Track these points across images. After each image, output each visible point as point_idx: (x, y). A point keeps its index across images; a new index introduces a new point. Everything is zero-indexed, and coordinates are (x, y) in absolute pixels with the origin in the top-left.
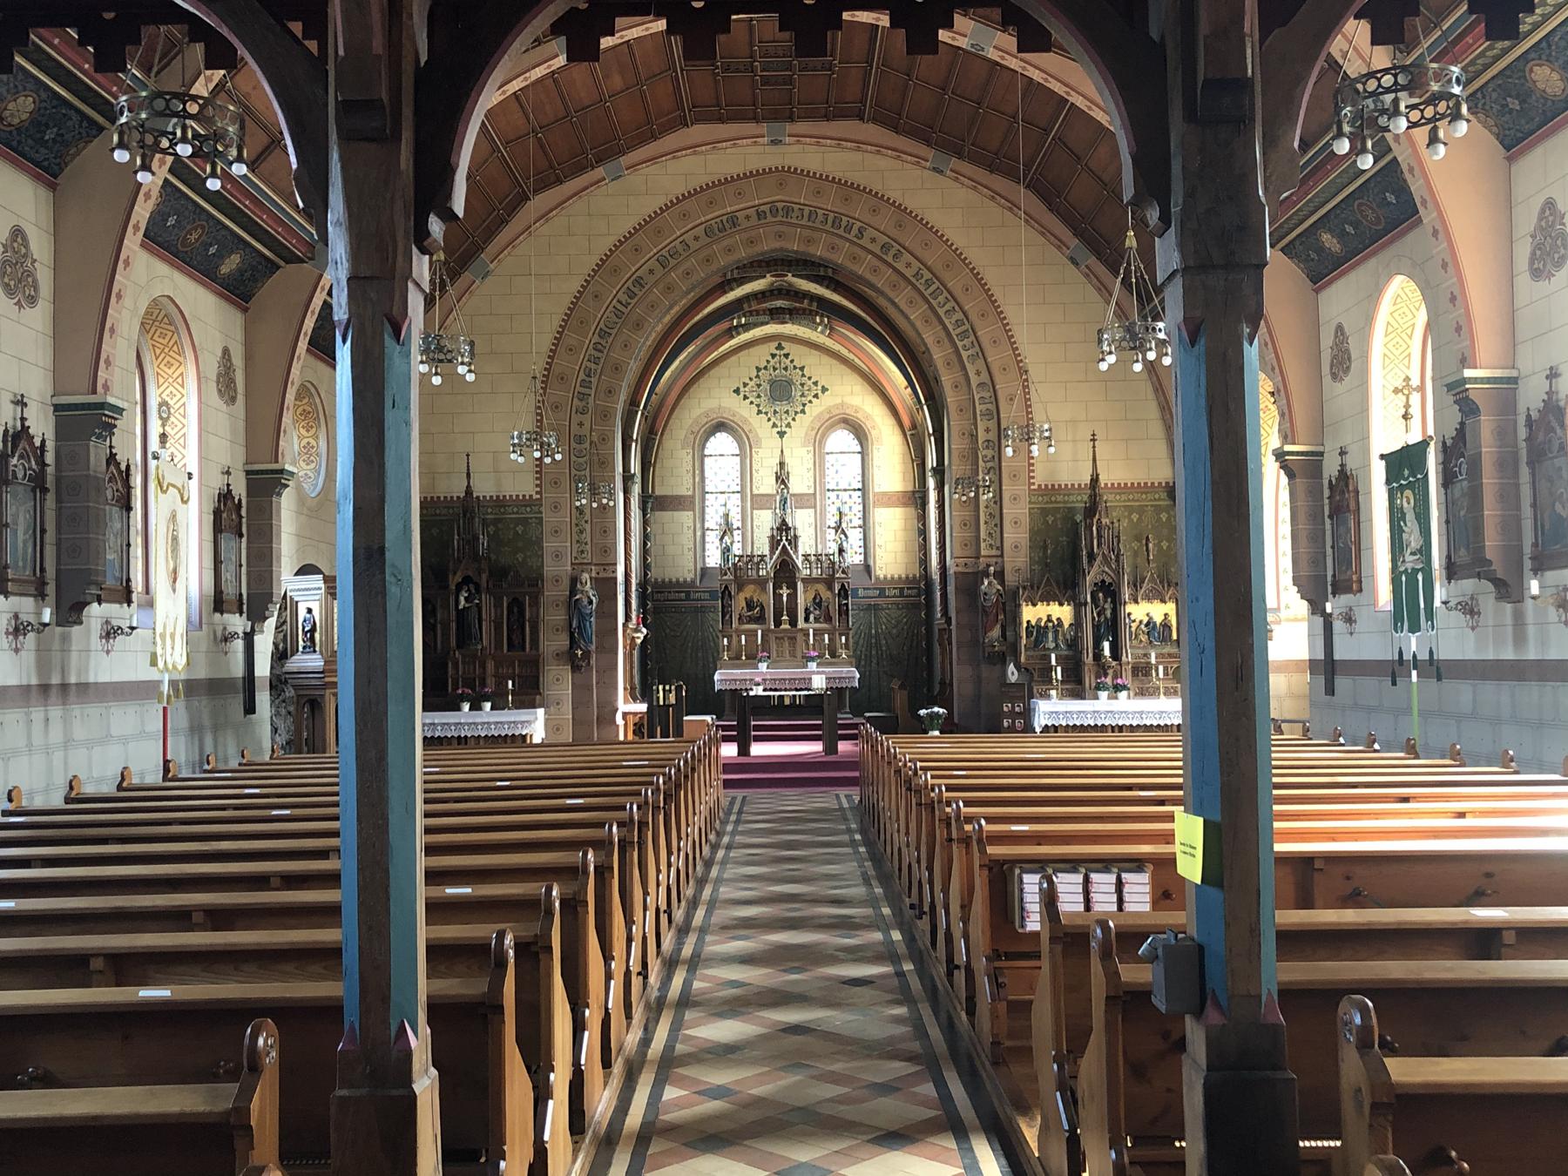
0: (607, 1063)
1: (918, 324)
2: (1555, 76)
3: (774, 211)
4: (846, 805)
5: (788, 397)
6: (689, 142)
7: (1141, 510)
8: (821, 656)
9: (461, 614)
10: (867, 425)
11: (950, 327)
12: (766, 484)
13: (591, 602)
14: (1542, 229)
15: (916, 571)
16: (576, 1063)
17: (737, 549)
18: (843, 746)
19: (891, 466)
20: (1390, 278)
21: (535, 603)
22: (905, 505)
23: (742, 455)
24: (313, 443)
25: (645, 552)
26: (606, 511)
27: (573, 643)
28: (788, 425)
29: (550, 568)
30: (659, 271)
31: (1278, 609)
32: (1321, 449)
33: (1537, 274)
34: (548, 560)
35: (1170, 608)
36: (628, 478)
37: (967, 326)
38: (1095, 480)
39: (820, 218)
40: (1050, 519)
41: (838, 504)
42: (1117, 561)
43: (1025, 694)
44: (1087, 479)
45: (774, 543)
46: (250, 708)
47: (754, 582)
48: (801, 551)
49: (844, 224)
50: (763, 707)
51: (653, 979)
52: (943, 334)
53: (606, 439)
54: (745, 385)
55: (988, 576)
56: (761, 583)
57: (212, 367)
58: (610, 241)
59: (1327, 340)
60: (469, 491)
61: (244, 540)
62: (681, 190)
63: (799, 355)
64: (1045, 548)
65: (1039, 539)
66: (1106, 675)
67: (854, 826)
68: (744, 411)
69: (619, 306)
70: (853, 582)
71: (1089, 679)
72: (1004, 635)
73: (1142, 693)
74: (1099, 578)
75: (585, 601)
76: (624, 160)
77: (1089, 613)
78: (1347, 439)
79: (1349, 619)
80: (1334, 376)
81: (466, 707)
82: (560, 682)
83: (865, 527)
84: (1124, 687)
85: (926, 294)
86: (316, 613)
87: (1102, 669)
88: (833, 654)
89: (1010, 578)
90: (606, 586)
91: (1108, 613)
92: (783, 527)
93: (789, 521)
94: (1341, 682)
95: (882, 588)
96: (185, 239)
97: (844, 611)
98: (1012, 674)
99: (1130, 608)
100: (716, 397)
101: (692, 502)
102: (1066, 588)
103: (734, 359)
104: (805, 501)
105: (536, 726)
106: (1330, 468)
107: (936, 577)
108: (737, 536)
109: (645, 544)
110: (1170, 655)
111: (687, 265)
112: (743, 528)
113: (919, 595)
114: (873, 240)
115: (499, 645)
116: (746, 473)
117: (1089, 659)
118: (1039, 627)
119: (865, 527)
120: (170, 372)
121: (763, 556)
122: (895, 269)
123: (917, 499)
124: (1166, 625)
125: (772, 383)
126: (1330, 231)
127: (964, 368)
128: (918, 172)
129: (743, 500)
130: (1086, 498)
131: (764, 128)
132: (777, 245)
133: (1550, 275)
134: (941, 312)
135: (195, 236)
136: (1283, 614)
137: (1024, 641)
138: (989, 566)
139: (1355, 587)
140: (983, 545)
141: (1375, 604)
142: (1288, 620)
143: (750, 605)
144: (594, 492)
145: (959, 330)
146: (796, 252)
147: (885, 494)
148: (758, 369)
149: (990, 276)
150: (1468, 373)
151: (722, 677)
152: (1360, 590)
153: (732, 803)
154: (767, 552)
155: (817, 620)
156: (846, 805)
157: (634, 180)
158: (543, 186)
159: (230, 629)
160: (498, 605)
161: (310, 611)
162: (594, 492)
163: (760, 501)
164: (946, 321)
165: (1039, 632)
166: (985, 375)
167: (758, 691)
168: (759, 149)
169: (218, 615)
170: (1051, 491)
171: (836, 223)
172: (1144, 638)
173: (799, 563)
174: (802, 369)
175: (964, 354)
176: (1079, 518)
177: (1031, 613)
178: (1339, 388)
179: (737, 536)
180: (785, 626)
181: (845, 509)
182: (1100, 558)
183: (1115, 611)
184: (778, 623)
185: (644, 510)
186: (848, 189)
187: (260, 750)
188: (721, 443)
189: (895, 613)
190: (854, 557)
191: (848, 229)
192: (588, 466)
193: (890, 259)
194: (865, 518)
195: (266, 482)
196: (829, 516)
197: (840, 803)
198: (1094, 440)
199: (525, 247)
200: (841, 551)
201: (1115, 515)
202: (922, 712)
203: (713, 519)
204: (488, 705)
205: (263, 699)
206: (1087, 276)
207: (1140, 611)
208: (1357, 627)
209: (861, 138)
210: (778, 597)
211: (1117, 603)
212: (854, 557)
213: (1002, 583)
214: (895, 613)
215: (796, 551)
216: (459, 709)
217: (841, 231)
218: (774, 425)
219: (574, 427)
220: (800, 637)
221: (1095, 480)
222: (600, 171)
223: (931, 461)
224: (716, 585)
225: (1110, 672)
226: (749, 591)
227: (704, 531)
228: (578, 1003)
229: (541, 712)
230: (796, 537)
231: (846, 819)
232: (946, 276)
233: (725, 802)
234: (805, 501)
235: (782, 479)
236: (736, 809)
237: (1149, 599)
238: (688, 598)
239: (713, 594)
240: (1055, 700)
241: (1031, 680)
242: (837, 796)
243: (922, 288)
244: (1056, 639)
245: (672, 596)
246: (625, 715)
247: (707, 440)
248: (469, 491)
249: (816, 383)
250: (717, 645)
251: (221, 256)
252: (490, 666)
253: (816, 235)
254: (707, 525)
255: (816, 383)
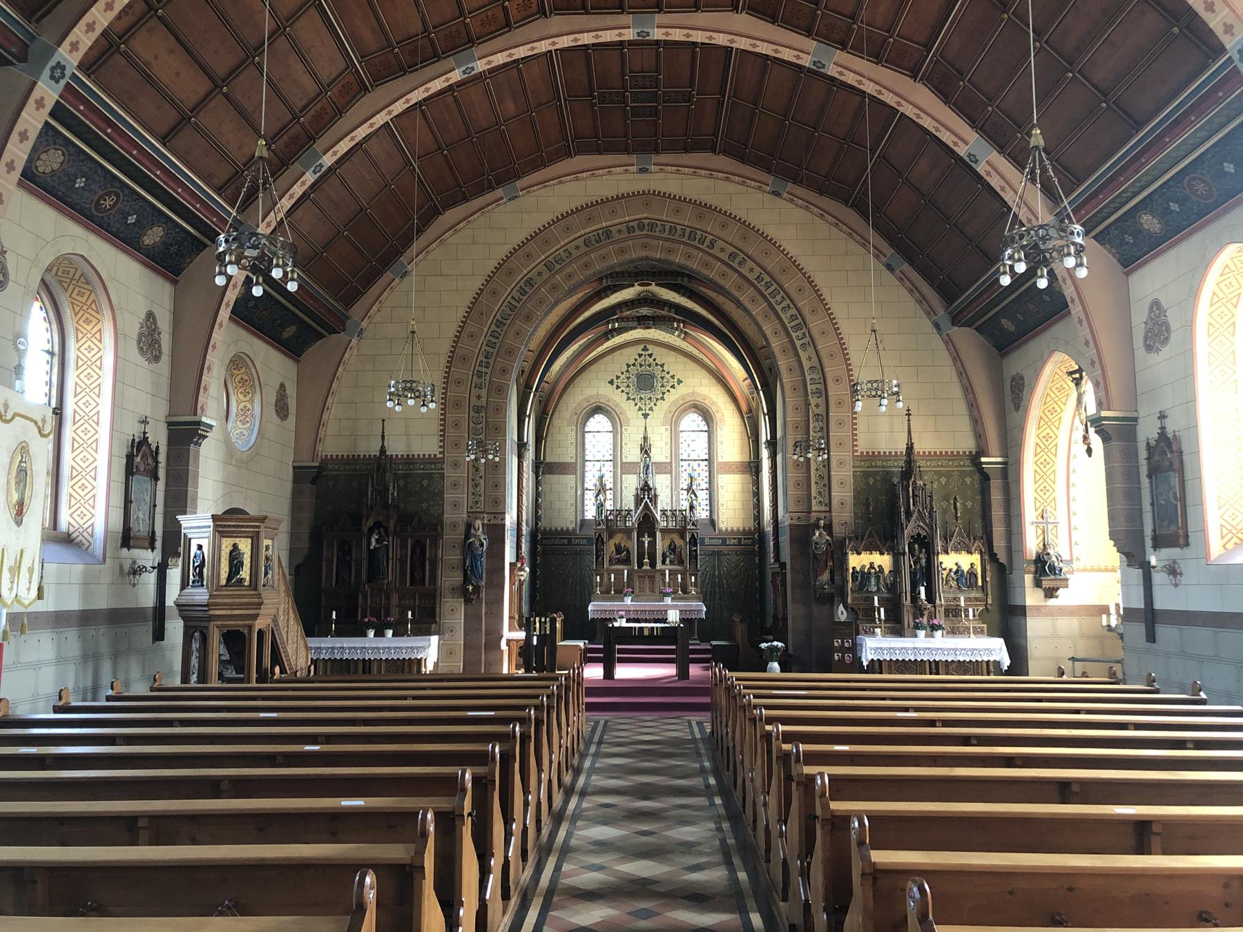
0: (506, 896)
1: (759, 319)
2: (1156, 221)
3: (641, 227)
4: (698, 736)
5: (651, 388)
6: (572, 170)
7: (948, 475)
8: (675, 592)
9: (372, 553)
10: (713, 409)
11: (786, 322)
12: (632, 454)
13: (482, 545)
14: (1152, 319)
15: (751, 525)
16: (506, 857)
17: (609, 505)
18: (695, 670)
19: (731, 442)
20: (1221, 248)
21: (435, 546)
22: (743, 472)
23: (614, 432)
24: (249, 406)
25: (537, 506)
26: (498, 469)
27: (466, 580)
28: (651, 409)
29: (449, 516)
30: (546, 275)
31: (1071, 561)
32: (1134, 415)
33: (1149, 348)
34: (447, 508)
35: (976, 558)
36: (521, 446)
37: (800, 320)
38: (910, 448)
39: (679, 232)
40: (871, 481)
41: (689, 470)
42: (931, 516)
43: (852, 630)
44: (902, 448)
45: (638, 500)
46: (159, 635)
47: (621, 531)
48: (659, 508)
49: (698, 237)
50: (625, 635)
51: (545, 831)
52: (779, 327)
53: (501, 410)
54: (618, 377)
55: (818, 528)
56: (628, 532)
57: (133, 326)
58: (505, 250)
59: (1139, 316)
60: (383, 450)
61: (161, 485)
62: (565, 207)
63: (661, 355)
64: (867, 505)
65: (863, 497)
66: (922, 615)
67: (707, 764)
68: (616, 398)
69: (514, 303)
70: (702, 533)
71: (908, 619)
72: (832, 579)
73: (954, 632)
74: (916, 532)
75: (477, 544)
76: (520, 183)
77: (907, 562)
78: (1166, 404)
79: (1173, 570)
80: (1149, 348)
81: (371, 633)
82: (454, 613)
83: (711, 490)
84: (939, 627)
85: (766, 293)
86: (205, 549)
87: (918, 611)
88: (685, 591)
89: (836, 529)
90: (496, 533)
91: (923, 561)
92: (646, 488)
93: (650, 483)
94: (1162, 631)
95: (724, 538)
96: (98, 203)
97: (693, 556)
98: (842, 614)
99: (942, 558)
100: (595, 387)
101: (574, 468)
102: (886, 541)
103: (610, 357)
104: (663, 468)
105: (430, 652)
106: (1147, 431)
107: (769, 529)
108: (609, 495)
109: (537, 500)
110: (976, 599)
111: (569, 270)
112: (614, 489)
113: (753, 544)
114: (722, 250)
115: (403, 581)
116: (617, 445)
117: (907, 602)
118: (862, 572)
119: (711, 490)
120: (89, 328)
121: (629, 511)
122: (740, 274)
123: (753, 468)
124: (972, 574)
125: (639, 376)
126: (1152, 213)
127: (797, 355)
128: (760, 195)
129: (614, 467)
130: (902, 463)
131: (634, 158)
132: (643, 253)
133: (1158, 350)
134: (778, 308)
135: (108, 203)
136: (1075, 565)
137: (850, 585)
138: (819, 519)
139: (1182, 541)
140: (814, 502)
141: (1207, 556)
142: (1078, 570)
143: (619, 549)
144: (482, 448)
145: (793, 324)
146: (659, 260)
147: (726, 464)
148: (628, 366)
149: (819, 280)
150: (983, 460)
151: (594, 608)
152: (1187, 544)
153: (594, 730)
154: (632, 508)
155: (672, 563)
156: (698, 736)
157: (527, 200)
158: (453, 202)
159: (140, 563)
160: (404, 546)
161: (200, 547)
162: (482, 448)
163: (628, 468)
164: (783, 316)
165: (863, 577)
166: (815, 359)
167: (623, 623)
168: (630, 176)
169: (125, 550)
170: (871, 457)
171: (692, 236)
172: (954, 584)
173: (658, 516)
174: (662, 366)
175: (798, 343)
176: (896, 480)
177: (857, 561)
178: (1154, 358)
179: (609, 495)
180: (647, 567)
181: (695, 475)
182: (915, 515)
183: (930, 561)
184: (640, 564)
185: (536, 473)
186: (703, 208)
187: (170, 672)
188: (598, 423)
189: (734, 558)
190: (702, 513)
191: (702, 241)
192: (487, 431)
193: (735, 265)
194: (710, 482)
195: (185, 433)
196: (682, 480)
197: (692, 732)
198: (909, 415)
199: (437, 253)
200: (692, 507)
201: (927, 478)
202: (764, 645)
203: (591, 481)
204: (390, 633)
205: (175, 628)
206: (901, 280)
207: (949, 561)
208: (1183, 580)
209: (713, 167)
210: (641, 544)
211: (931, 554)
212: (702, 513)
213: (830, 534)
214: (734, 558)
215: (656, 507)
216: (365, 635)
217: (696, 243)
218: (640, 409)
219: (473, 399)
220: (658, 577)
221: (910, 448)
222: (499, 192)
223: (764, 435)
224: (591, 533)
225: (926, 613)
226: (618, 539)
227: (584, 489)
228: (484, 855)
229: (434, 639)
230: (656, 496)
231: (699, 755)
232: (782, 278)
233: (586, 729)
234: (663, 468)
235: (645, 450)
236: (596, 739)
237: (957, 550)
238: (570, 544)
239: (589, 539)
240: (879, 637)
241: (857, 619)
242: (689, 722)
243: (762, 289)
244: (878, 583)
245: (557, 542)
246: (509, 641)
247: (587, 420)
248: (383, 450)
249: (673, 377)
250: (591, 581)
251: (141, 226)
252: (395, 599)
253: (676, 246)
254: (586, 486)
255: (673, 377)
